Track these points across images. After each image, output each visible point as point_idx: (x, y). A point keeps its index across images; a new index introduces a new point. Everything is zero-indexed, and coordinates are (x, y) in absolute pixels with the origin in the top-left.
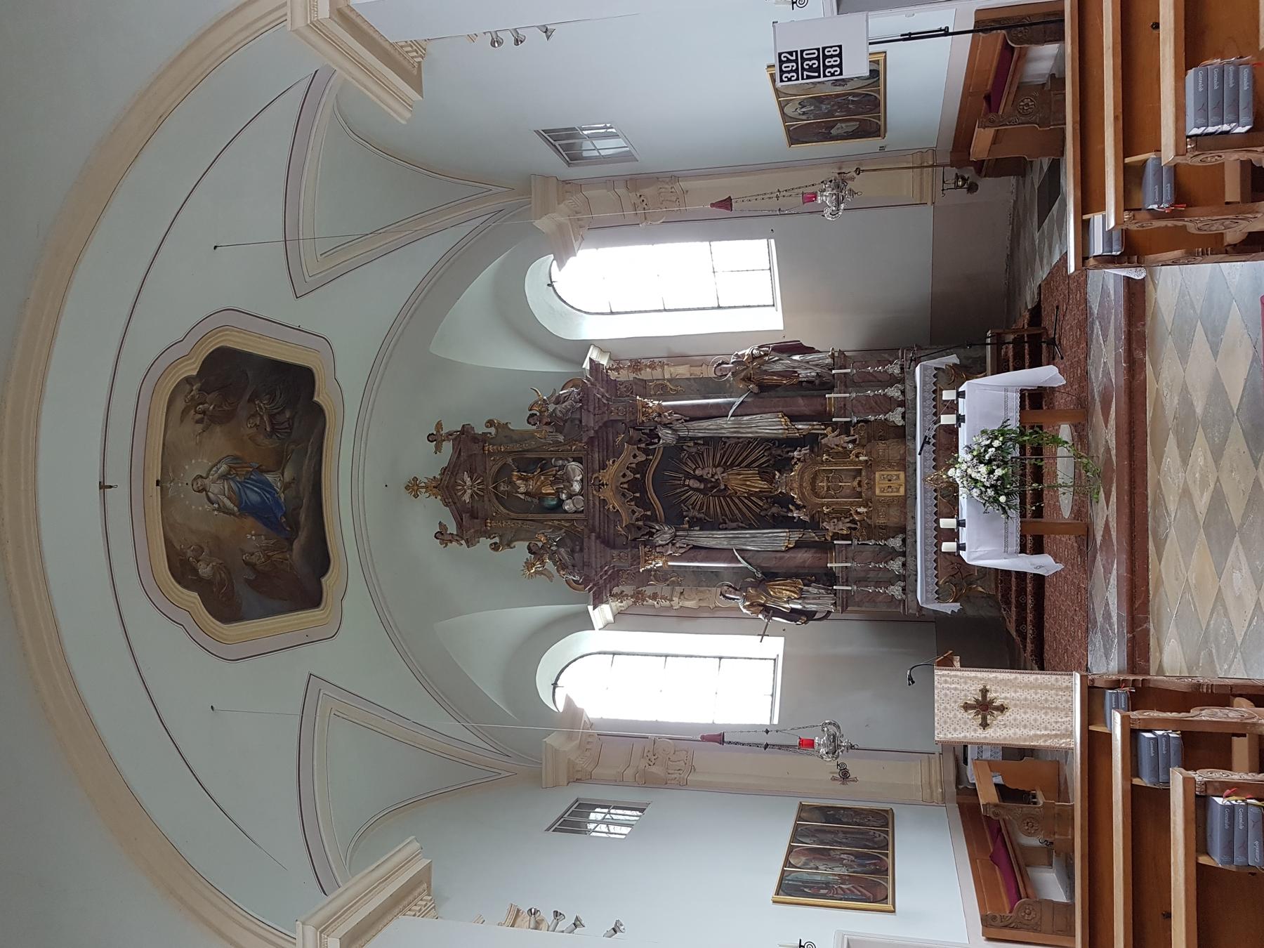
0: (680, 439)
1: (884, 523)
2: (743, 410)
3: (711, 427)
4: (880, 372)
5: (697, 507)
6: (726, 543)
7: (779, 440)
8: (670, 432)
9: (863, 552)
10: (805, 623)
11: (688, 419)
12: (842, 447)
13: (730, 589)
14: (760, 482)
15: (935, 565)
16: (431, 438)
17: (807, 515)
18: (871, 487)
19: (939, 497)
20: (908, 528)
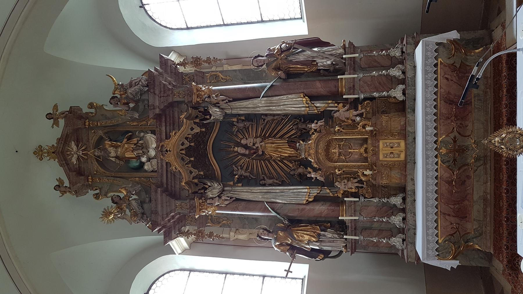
0: (226, 115)
1: (387, 183)
2: (272, 92)
3: (249, 106)
4: (384, 55)
5: (245, 168)
6: (260, 197)
7: (304, 116)
8: (218, 110)
9: (368, 206)
10: (323, 259)
11: (231, 99)
12: (352, 120)
13: (265, 232)
14: (289, 149)
15: (436, 225)
16: (49, 116)
17: (322, 176)
18: (376, 153)
19: (439, 162)
20: (409, 188)
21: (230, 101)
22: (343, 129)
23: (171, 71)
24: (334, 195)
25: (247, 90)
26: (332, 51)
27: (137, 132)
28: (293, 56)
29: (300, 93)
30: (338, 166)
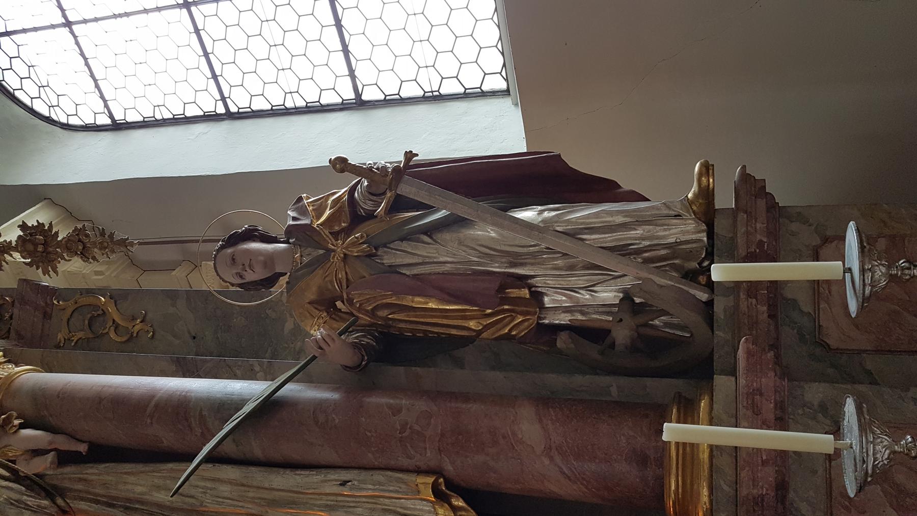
11: (83, 448)
25: (149, 410)
26: (623, 226)
28: (405, 244)
29: (419, 471)
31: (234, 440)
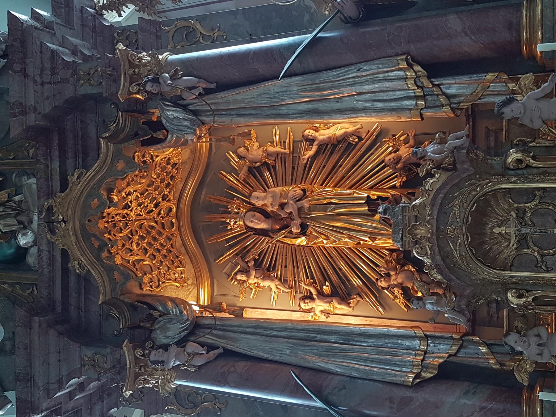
11: (213, 86)
17: (461, 312)
21: (208, 91)
22: (534, 158)
23: (82, 22)
24: (504, 365)
25: (250, 56)
27: (14, 175)
29: (398, 55)
30: (514, 280)
31: (299, 61)
